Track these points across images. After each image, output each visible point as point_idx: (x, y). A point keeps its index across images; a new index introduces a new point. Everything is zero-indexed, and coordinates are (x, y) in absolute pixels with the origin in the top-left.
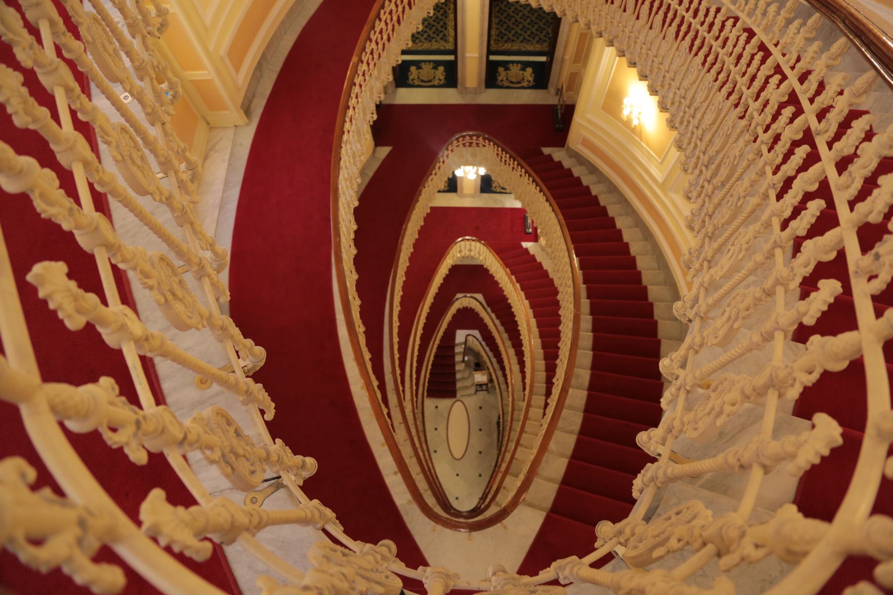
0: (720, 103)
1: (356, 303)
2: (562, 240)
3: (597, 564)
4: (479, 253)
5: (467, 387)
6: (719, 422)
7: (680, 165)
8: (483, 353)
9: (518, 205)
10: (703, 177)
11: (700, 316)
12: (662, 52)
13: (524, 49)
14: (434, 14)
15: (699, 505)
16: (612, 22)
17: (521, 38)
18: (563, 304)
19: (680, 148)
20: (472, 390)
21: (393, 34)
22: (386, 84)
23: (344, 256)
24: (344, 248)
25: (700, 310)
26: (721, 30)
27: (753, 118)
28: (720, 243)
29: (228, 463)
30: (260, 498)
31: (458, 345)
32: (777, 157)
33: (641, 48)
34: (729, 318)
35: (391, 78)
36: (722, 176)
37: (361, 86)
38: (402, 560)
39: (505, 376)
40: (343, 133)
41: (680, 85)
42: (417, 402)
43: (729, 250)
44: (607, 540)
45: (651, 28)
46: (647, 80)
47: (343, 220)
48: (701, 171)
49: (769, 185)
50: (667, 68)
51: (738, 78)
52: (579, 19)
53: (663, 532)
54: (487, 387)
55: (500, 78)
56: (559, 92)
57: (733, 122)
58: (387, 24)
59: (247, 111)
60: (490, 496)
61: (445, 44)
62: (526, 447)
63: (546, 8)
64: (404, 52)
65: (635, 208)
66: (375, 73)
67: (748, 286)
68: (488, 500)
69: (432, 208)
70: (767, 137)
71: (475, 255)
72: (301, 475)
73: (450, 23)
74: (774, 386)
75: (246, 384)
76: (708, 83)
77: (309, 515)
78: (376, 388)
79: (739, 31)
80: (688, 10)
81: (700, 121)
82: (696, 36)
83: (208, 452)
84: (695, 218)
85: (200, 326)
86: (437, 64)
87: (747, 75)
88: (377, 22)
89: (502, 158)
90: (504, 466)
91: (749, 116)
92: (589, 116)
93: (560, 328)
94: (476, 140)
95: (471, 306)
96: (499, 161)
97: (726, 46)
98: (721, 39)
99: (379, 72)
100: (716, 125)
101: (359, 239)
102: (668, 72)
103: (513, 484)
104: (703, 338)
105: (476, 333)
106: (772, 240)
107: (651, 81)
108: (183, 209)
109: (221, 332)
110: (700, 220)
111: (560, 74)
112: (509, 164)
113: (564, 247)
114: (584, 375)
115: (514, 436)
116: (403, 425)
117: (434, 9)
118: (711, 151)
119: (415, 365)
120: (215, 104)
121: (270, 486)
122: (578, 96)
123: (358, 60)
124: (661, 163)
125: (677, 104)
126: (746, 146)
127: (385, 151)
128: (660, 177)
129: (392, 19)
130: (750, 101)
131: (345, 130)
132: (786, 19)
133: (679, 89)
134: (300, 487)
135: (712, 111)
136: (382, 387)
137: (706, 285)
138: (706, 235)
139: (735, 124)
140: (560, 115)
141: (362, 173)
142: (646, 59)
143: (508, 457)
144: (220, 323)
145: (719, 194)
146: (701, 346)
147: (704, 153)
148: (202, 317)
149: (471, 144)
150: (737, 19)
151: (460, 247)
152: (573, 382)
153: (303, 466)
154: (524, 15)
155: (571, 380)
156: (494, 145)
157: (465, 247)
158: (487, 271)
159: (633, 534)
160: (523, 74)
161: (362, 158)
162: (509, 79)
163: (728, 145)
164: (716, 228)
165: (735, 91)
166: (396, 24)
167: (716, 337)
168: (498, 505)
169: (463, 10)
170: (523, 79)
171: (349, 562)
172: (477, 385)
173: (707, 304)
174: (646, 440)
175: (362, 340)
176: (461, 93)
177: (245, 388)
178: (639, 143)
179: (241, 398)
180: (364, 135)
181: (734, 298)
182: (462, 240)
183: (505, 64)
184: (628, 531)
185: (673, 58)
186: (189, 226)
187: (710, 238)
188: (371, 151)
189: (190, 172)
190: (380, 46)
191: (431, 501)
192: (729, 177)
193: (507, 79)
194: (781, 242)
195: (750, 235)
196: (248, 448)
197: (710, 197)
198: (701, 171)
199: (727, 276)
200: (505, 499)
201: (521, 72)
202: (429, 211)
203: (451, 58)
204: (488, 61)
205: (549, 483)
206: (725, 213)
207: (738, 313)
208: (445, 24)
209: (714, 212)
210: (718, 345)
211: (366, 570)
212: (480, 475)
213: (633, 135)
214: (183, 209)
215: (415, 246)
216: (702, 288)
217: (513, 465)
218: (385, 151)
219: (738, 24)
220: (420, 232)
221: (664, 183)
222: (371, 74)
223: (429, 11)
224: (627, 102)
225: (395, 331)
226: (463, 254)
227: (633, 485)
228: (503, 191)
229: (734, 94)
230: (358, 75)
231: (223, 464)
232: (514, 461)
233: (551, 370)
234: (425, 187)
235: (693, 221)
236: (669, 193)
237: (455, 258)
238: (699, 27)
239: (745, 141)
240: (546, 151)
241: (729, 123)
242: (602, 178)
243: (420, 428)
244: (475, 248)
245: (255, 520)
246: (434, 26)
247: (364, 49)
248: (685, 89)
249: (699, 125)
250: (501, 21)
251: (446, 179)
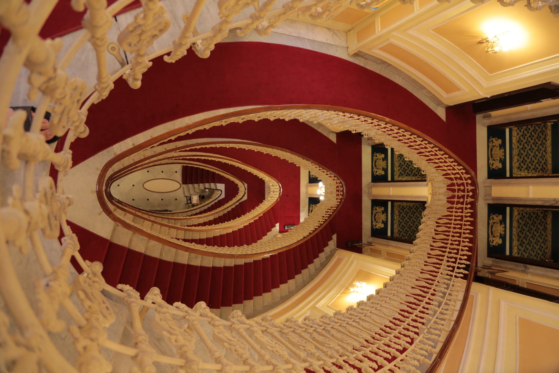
0: (362, 336)
1: (239, 120)
2: (280, 247)
3: (73, 261)
4: (272, 197)
5: (189, 191)
6: (165, 333)
7: (325, 314)
8: (211, 200)
9: (302, 220)
10: (318, 327)
11: (232, 325)
12: (393, 302)
13: (395, 222)
14: (415, 168)
15: (112, 320)
16: (410, 273)
17: (401, 221)
18: (241, 248)
19: (336, 314)
20: (187, 194)
21: (403, 143)
22: (373, 138)
23: (269, 113)
24: (274, 113)
25: (236, 325)
26: (404, 335)
27: (352, 354)
28: (277, 336)
29: (135, 29)
30: (115, 52)
31: (215, 185)
32: (328, 367)
33: (395, 290)
34: (230, 340)
35: (377, 142)
36: (318, 337)
37: (372, 123)
38: (76, 140)
39: (196, 214)
40: (344, 113)
41: (372, 313)
42: (179, 159)
43: (273, 341)
44: (91, 268)
45: (407, 295)
46: (376, 294)
47: (291, 112)
48: (321, 326)
49: (312, 363)
50: (383, 305)
51: (376, 345)
52: (412, 254)
53: (94, 297)
54: (189, 203)
55: (377, 208)
56: (370, 244)
57: (350, 343)
58: (408, 139)
59: (356, 55)
60: (120, 205)
61: (397, 175)
62: (151, 228)
63: (418, 234)
64: (392, 149)
65: (300, 291)
66: (380, 132)
67: (249, 350)
68: (118, 204)
69: (299, 167)
70: (341, 362)
71: (271, 194)
72: (129, 77)
73: (410, 178)
74: (187, 363)
75: (186, 44)
76: (374, 328)
77: (104, 80)
78: (187, 132)
79: (404, 345)
80: (416, 316)
81: (351, 325)
82: (401, 321)
83: (142, 16)
84: (293, 323)
85: (221, 15)
86: (386, 170)
87: (378, 350)
88: (410, 133)
89: (330, 210)
90: (140, 214)
91: (354, 352)
92: (355, 263)
93: (226, 246)
94: (341, 194)
95: (240, 192)
96: (328, 208)
97: (395, 338)
98: (399, 335)
99: (380, 135)
100: (348, 334)
101: (279, 122)
102: (381, 306)
103: (128, 219)
104: (218, 326)
105: (223, 196)
106: (278, 364)
107: (375, 296)
108: (293, 8)
109: (218, 28)
110: (291, 326)
111: (380, 244)
112: (326, 214)
113: (276, 248)
114: (197, 261)
115: (159, 220)
116: (164, 150)
117: (418, 168)
118: (333, 332)
119: (203, 158)
120: (361, 35)
121: (123, 59)
122: (367, 255)
123: (387, 122)
124: (328, 306)
125: (362, 311)
126: (336, 350)
127: (333, 139)
128: (319, 305)
129: (411, 142)
130: (362, 352)
131: (345, 114)
132: (410, 370)
133: (371, 312)
134: (122, 76)
135: (357, 332)
136: (188, 137)
137: (251, 328)
138: (282, 329)
139: (349, 344)
140: (356, 245)
141: (320, 125)
142: (389, 293)
143: (146, 216)
144: (224, 28)
145: (307, 336)
146: (214, 325)
147: (332, 328)
148: (227, 16)
149: (338, 191)
150: (411, 344)
151: (276, 185)
152: (193, 255)
153: (135, 79)
154: (415, 222)
155: (194, 253)
156: (337, 205)
157: (275, 188)
158: (261, 202)
159: (94, 282)
160: (380, 222)
161: (329, 124)
162: (377, 213)
163: (336, 341)
164: (286, 334)
165: (368, 344)
166: (408, 145)
167: (218, 333)
168: (115, 210)
170: (377, 222)
171: (73, 103)
172: (190, 197)
173: (239, 329)
174: (155, 294)
175: (217, 124)
176: (368, 185)
177: (183, 43)
178: (339, 293)
179: (177, 40)
180: (343, 125)
181: (243, 343)
182: (280, 186)
183: (386, 211)
184: (96, 279)
185: (388, 309)
186: (284, 11)
187: (280, 331)
188: (333, 130)
189: (316, 15)
190: (395, 135)
191: (117, 167)
192: (317, 341)
193: (377, 212)
194: (277, 369)
195: (281, 352)
196: (145, 42)
197: (305, 331)
198: (321, 326)
199: (257, 341)
200: (119, 214)
201: (381, 221)
202: (297, 166)
203: (389, 179)
204: (505, 206)
205: (129, 241)
206: (295, 339)
207: (233, 345)
208: (409, 175)
209: (296, 333)
210: (214, 333)
211: (69, 112)
212: (133, 200)
213: (344, 289)
214: (293, 8)
215: (276, 157)
216: (249, 326)
217: (140, 219)
218: (333, 139)
219: (408, 345)
220: (284, 160)
221: (316, 308)
222: (379, 129)
223: (416, 165)
224: (364, 284)
225: (223, 145)
226: (271, 187)
227: (126, 284)
228: (310, 211)
229: (367, 343)
230: (378, 122)
231: (135, 25)
232: (143, 220)
233: (200, 242)
234: (312, 163)
235: (291, 322)
236: (310, 311)
237: (269, 182)
238: (407, 322)
239: (338, 350)
240: (335, 237)
241: (350, 341)
242: (318, 271)
243: (163, 162)
244: (275, 195)
245: (99, 43)
246: (408, 168)
247: (394, 125)
248: (371, 316)
249: (349, 324)
250: (411, 208)
251: (317, 176)
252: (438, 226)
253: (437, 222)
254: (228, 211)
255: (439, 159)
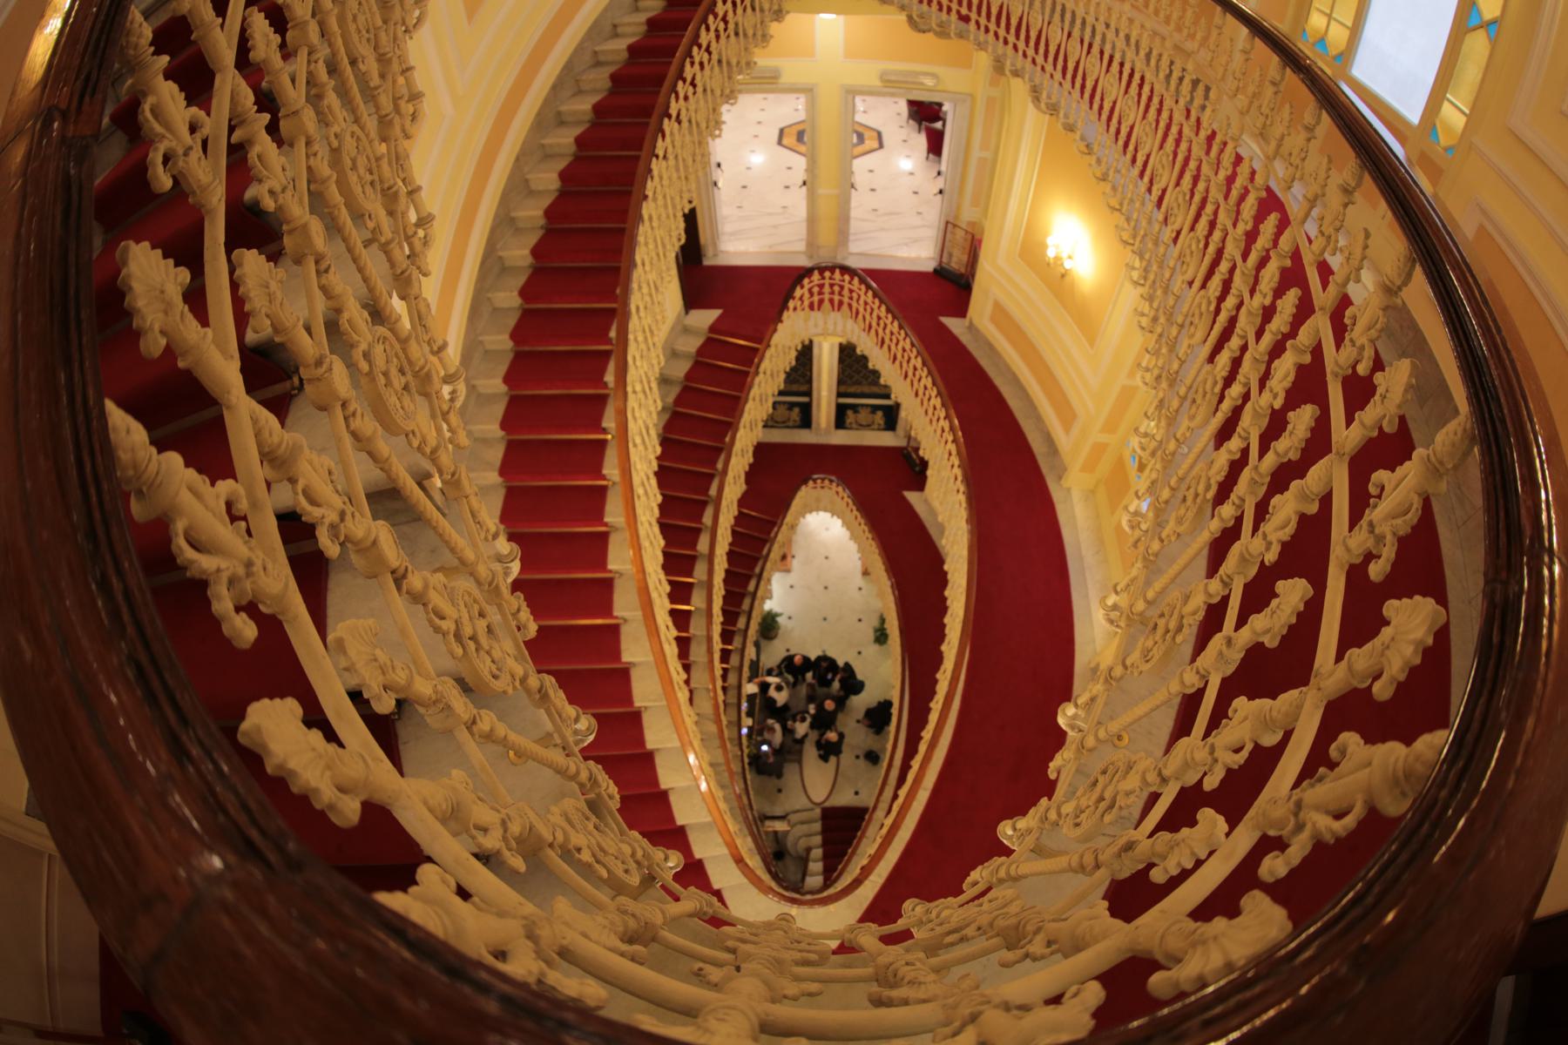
127: (705, 318)
183: (854, 408)
203: (804, 399)
218: (705, 318)
254: (923, 742)
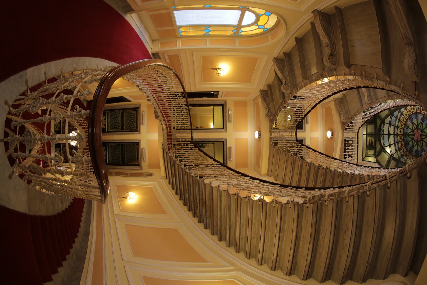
169: (133, 134)
252: (84, 153)
253: (83, 151)
255: (84, 124)
